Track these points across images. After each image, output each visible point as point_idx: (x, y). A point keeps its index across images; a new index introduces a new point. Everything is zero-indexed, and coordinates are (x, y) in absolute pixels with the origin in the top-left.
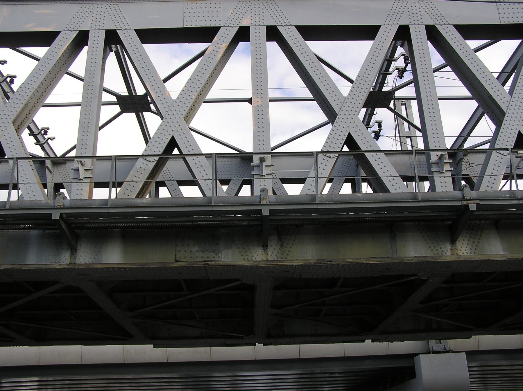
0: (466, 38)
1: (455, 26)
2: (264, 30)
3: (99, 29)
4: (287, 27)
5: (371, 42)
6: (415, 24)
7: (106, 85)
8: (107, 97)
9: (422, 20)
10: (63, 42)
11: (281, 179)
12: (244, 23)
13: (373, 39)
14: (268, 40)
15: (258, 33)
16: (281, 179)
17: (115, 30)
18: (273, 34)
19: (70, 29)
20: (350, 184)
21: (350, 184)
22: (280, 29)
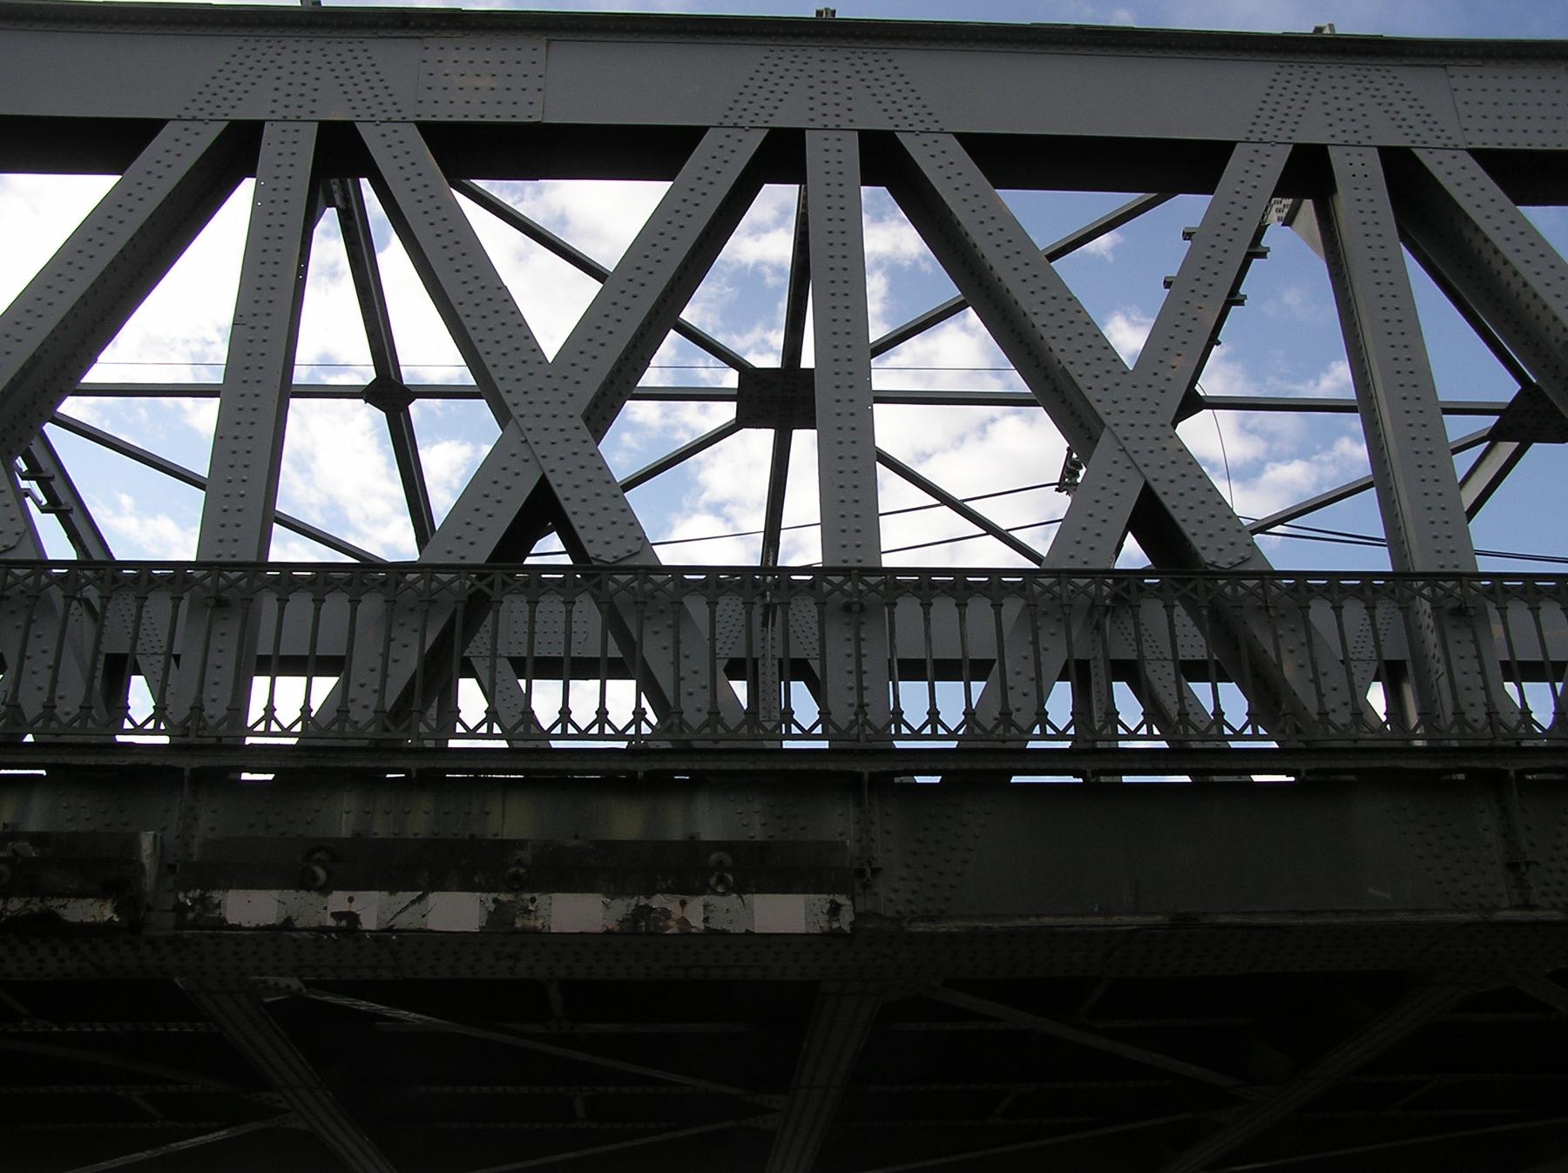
0: (1520, 200)
1: (963, 138)
2: (852, 145)
3: (298, 120)
4: (925, 138)
5: (1206, 199)
6: (826, 128)
7: (1447, 393)
8: (1458, 428)
9: (851, 115)
10: (170, 160)
11: (1147, 494)
12: (785, 119)
13: (1209, 190)
14: (866, 181)
15: (834, 154)
16: (1147, 494)
17: (352, 123)
18: (885, 161)
19: (200, 115)
20: (772, 432)
21: (772, 432)
22: (910, 144)
